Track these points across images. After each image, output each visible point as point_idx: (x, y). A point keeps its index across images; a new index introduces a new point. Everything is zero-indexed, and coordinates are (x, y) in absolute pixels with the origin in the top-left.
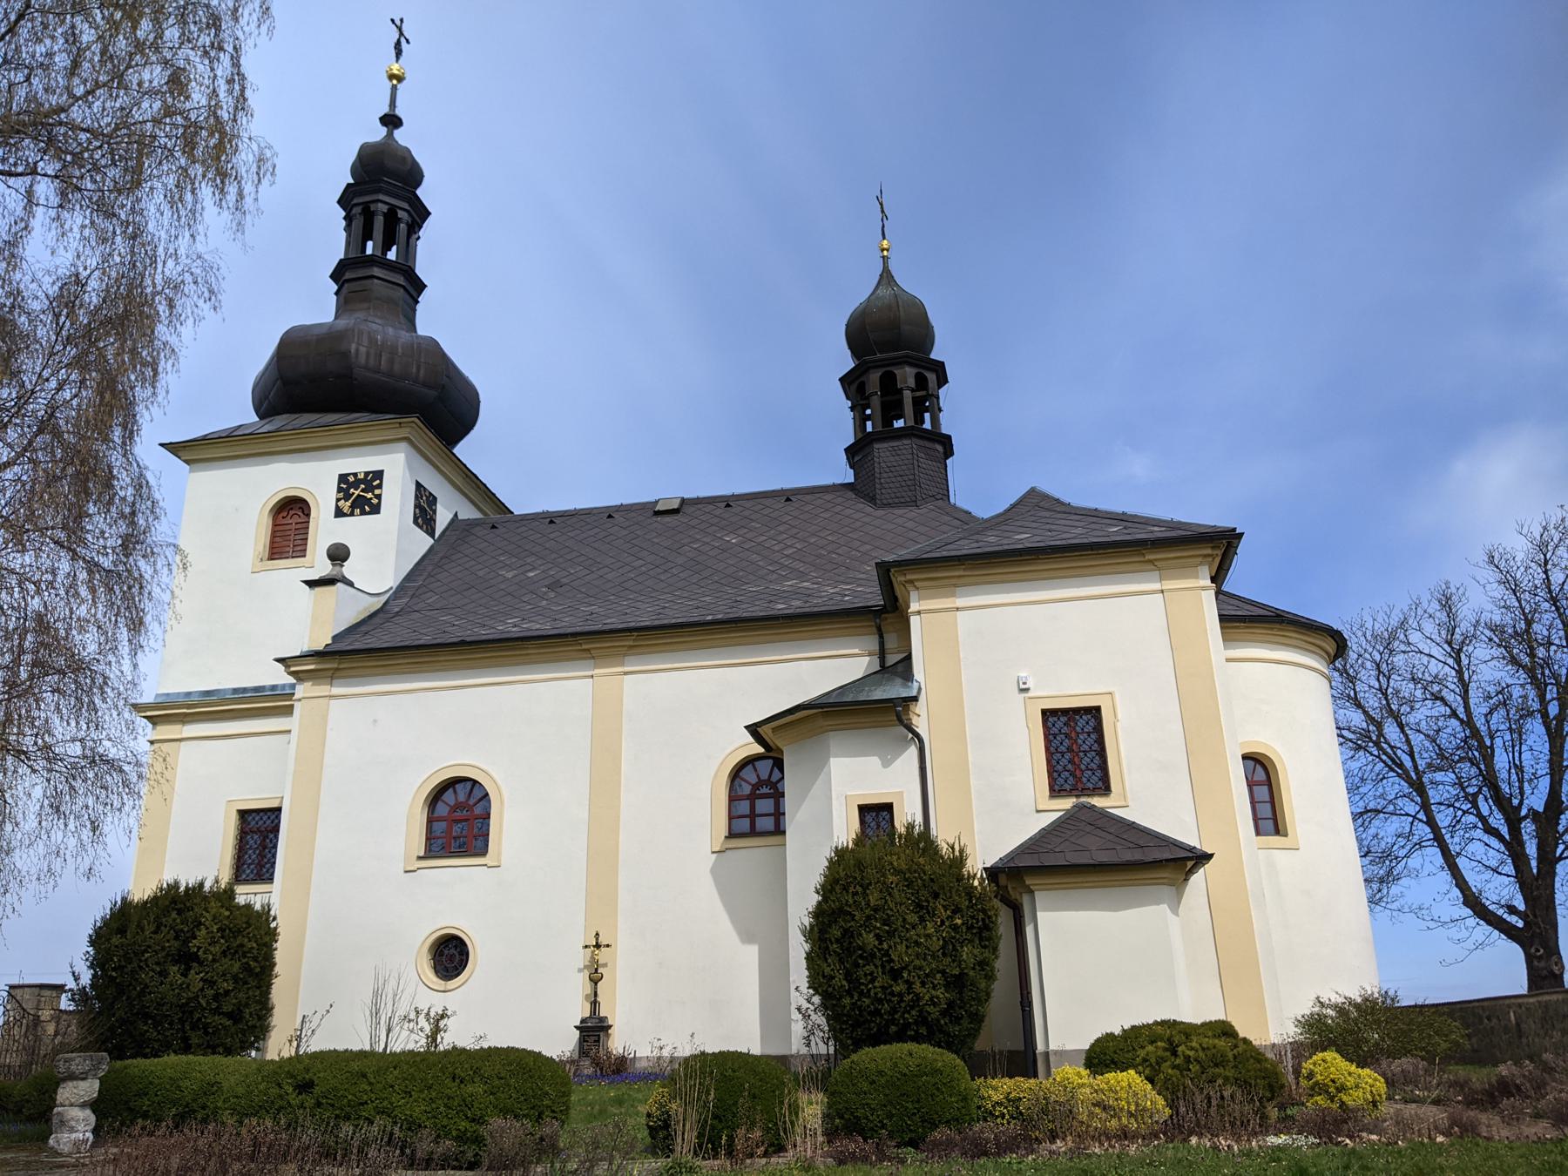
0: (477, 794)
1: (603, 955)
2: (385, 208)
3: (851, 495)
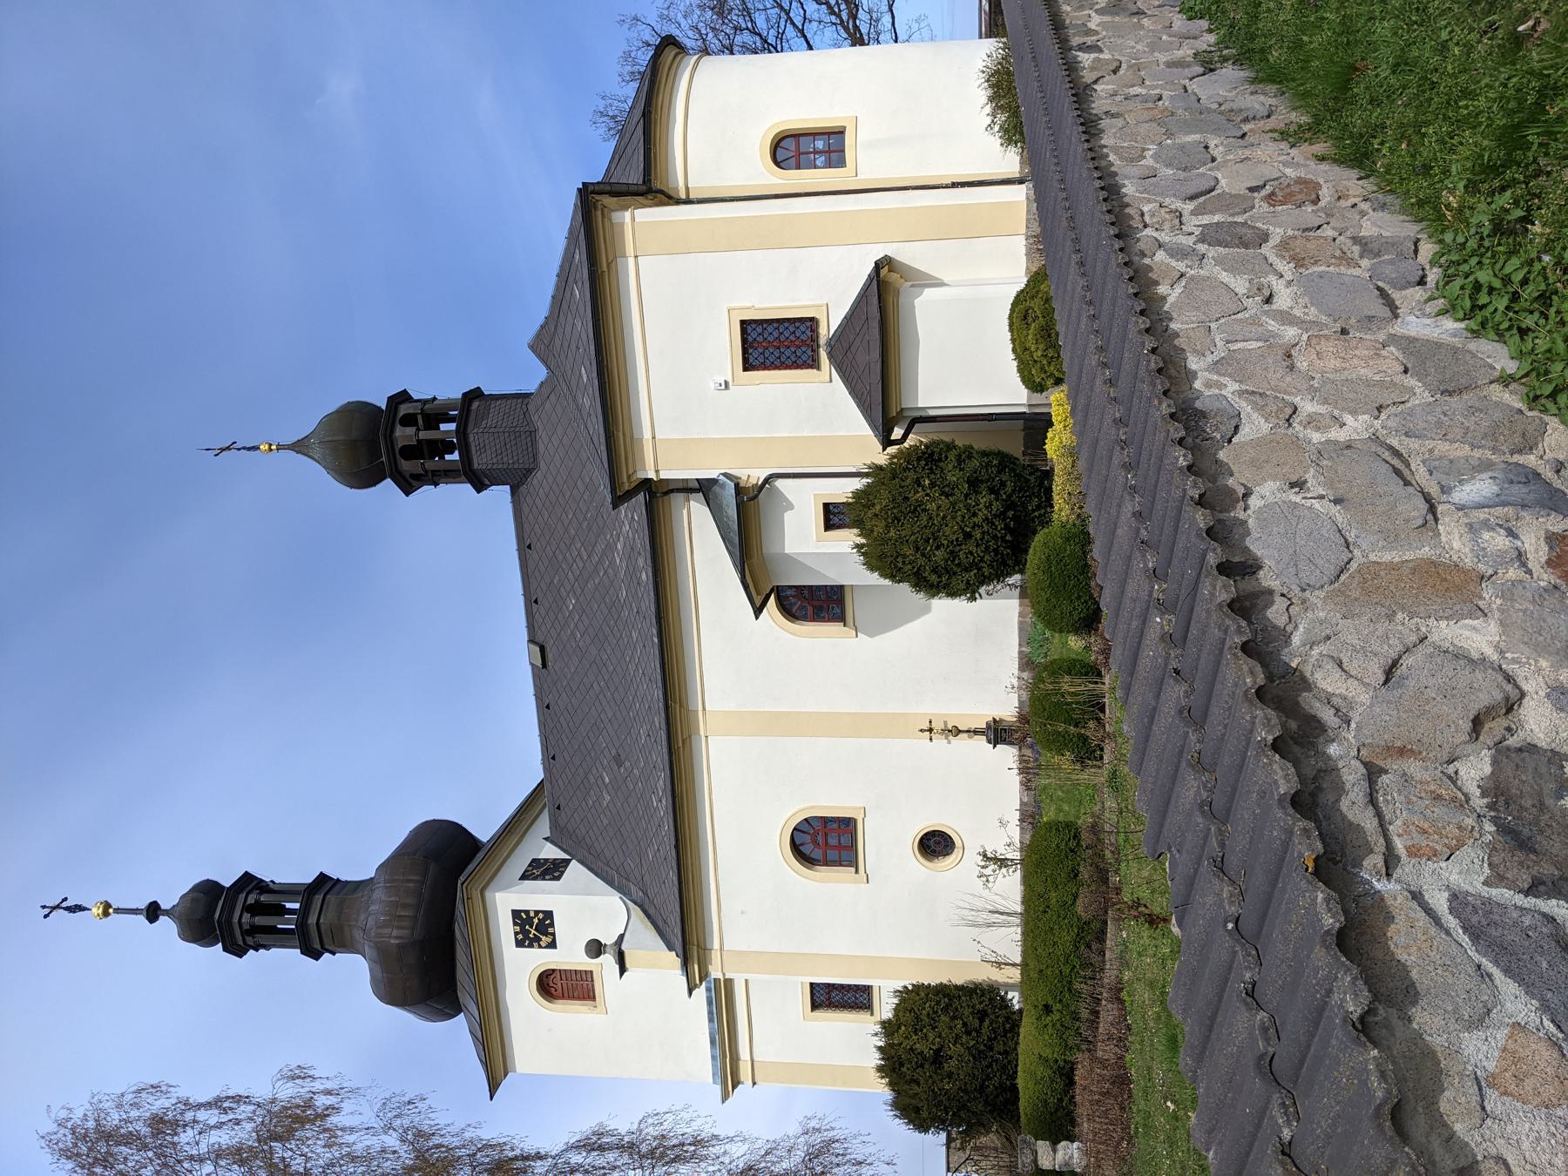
0: (806, 827)
1: (937, 726)
2: (246, 917)
3: (523, 489)
